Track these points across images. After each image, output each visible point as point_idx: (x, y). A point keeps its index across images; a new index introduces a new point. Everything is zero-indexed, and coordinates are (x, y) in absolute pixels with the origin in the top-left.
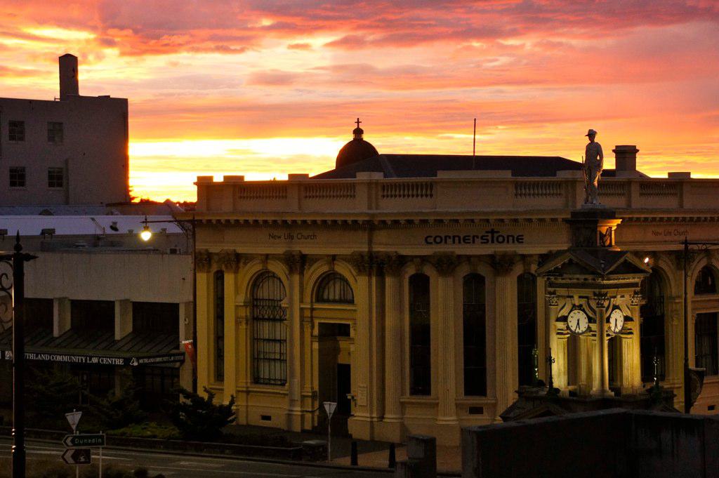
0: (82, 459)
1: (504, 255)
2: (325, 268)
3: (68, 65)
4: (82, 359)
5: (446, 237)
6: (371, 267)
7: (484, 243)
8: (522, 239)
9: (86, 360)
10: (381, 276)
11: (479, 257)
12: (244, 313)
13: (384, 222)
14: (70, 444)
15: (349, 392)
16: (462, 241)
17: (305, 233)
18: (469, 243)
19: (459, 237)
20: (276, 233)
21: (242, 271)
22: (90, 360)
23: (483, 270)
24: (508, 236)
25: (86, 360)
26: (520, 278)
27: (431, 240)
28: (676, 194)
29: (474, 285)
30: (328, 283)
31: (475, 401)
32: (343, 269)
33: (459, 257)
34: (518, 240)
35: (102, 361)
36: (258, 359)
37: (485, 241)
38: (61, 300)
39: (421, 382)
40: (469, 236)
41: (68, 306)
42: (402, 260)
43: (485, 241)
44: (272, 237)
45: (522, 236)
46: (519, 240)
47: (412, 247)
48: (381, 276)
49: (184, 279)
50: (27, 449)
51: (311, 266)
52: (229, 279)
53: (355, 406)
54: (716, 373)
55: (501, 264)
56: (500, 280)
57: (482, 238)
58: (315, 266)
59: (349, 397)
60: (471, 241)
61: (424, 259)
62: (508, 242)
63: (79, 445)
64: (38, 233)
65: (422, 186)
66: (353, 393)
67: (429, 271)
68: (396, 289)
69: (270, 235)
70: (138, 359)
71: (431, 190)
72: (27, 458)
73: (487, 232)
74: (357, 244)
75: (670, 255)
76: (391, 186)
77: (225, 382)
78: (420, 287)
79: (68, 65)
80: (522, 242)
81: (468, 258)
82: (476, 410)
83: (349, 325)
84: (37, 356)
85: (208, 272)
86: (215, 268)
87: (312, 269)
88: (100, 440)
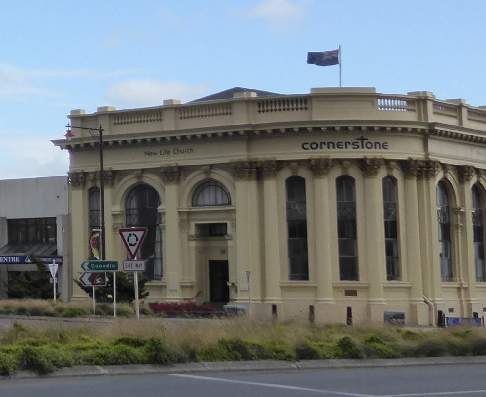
0: (98, 281)
1: (319, 160)
2: (202, 177)
5: (321, 143)
7: (356, 148)
8: (387, 146)
12: (121, 221)
14: (87, 268)
16: (336, 146)
17: (183, 147)
18: (342, 148)
19: (379, 144)
20: (152, 150)
23: (303, 173)
24: (376, 143)
26: (384, 180)
27: (306, 146)
31: (350, 284)
32: (220, 176)
33: (334, 160)
34: (383, 146)
37: (355, 144)
40: (342, 142)
42: (280, 165)
43: (356, 147)
44: (148, 154)
45: (387, 143)
46: (384, 146)
49: (58, 197)
52: (107, 192)
54: (484, 281)
56: (369, 181)
60: (344, 147)
61: (300, 162)
63: (95, 269)
67: (354, 172)
69: (146, 152)
71: (306, 104)
73: (357, 139)
75: (184, 300)
77: (461, 98)
81: (340, 162)
82: (351, 293)
83: (226, 224)
85: (83, 188)
88: (114, 266)
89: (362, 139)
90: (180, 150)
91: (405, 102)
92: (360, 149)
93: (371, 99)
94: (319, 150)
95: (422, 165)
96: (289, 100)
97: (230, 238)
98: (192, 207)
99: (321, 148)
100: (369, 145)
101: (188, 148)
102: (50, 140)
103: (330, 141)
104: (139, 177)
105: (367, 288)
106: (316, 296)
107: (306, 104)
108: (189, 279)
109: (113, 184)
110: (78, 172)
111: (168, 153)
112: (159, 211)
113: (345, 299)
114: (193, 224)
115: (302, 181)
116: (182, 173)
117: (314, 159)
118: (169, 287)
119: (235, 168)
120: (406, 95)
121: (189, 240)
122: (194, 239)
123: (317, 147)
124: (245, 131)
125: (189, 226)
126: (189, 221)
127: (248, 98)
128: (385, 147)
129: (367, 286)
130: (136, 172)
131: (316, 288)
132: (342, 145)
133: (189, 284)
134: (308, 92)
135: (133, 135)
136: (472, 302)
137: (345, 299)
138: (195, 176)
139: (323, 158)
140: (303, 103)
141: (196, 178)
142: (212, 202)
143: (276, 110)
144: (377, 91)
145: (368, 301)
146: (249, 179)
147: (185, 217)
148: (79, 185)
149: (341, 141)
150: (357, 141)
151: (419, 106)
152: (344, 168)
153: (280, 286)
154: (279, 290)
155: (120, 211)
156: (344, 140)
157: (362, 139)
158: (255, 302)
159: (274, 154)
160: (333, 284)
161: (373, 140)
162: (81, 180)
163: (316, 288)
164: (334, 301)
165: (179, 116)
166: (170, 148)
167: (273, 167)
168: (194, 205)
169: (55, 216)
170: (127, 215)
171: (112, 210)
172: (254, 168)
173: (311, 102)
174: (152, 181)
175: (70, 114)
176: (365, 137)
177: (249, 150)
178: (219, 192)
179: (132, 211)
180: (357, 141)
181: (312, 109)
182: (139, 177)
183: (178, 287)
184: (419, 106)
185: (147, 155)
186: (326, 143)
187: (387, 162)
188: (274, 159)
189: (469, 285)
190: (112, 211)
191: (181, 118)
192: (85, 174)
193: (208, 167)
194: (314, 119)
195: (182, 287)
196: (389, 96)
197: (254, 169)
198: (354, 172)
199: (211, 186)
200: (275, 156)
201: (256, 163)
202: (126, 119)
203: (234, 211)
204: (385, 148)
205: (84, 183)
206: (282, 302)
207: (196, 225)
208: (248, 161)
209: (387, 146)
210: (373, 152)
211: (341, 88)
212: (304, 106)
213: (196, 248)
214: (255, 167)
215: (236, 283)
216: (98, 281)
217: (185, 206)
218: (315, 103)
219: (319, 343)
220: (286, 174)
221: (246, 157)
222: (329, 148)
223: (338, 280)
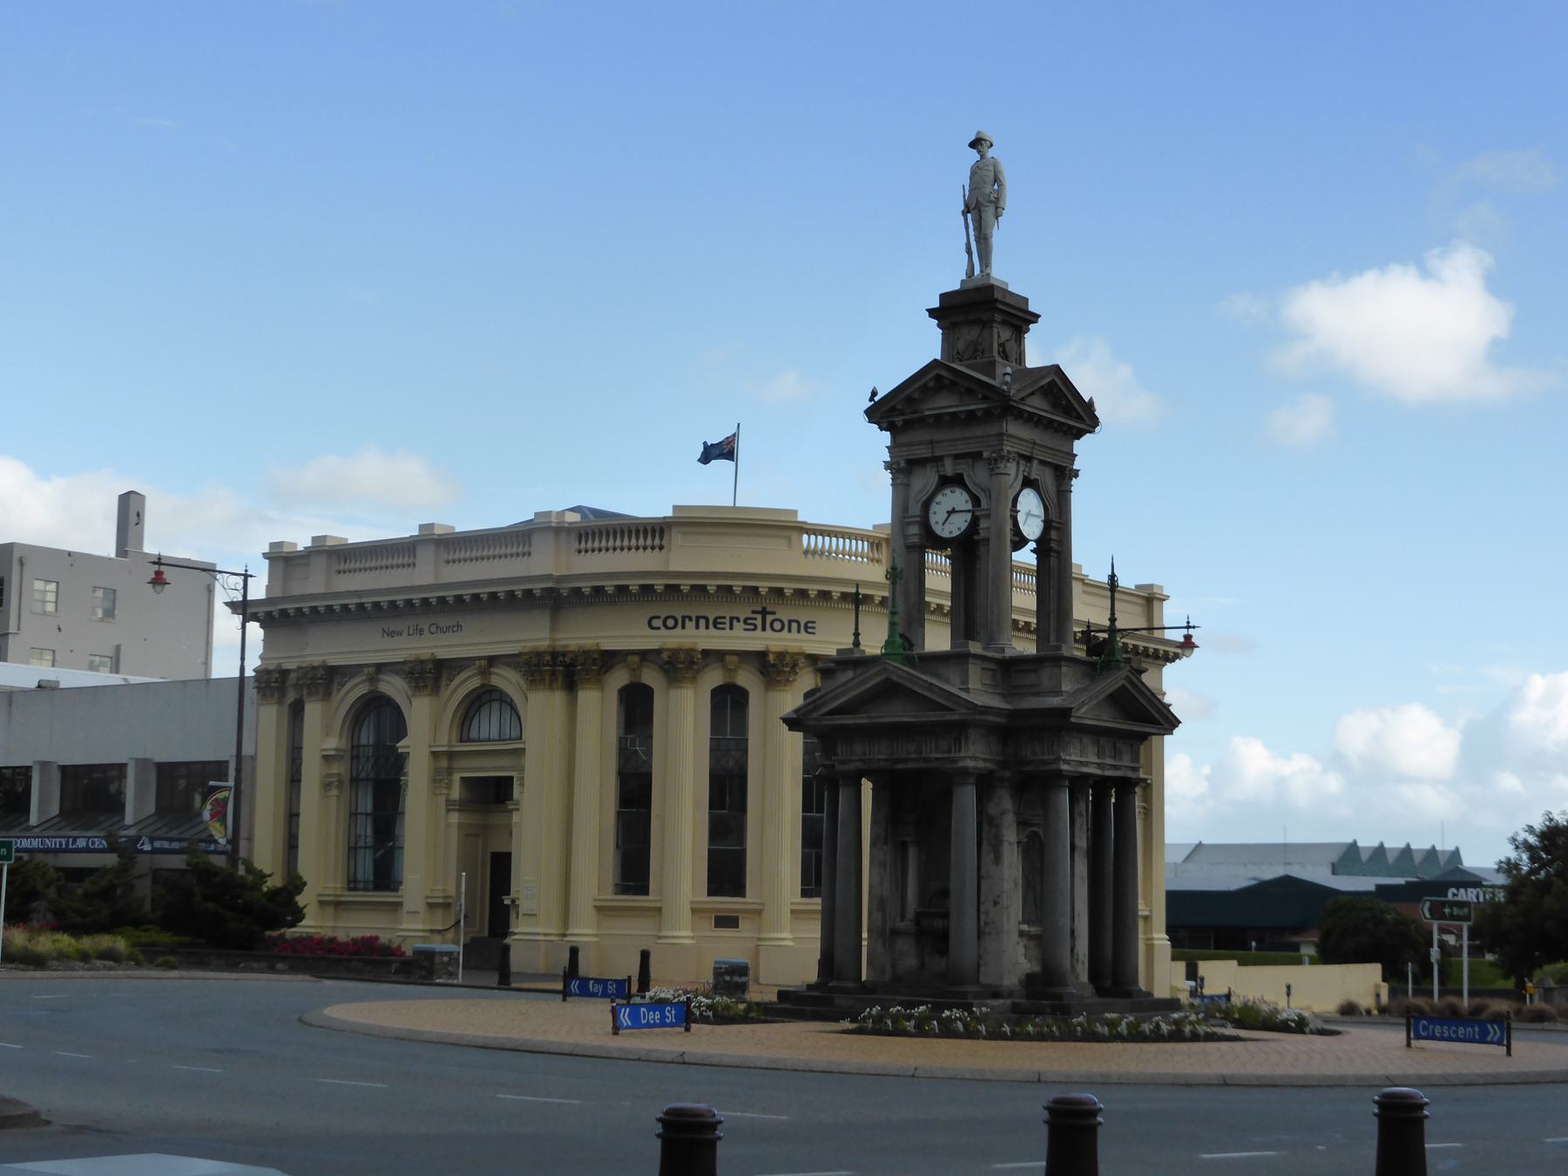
1: (675, 652)
2: (475, 683)
3: (130, 510)
4: (61, 844)
5: (684, 618)
6: (553, 673)
8: (814, 628)
9: (67, 843)
10: (571, 687)
11: (744, 656)
13: (577, 591)
15: (508, 893)
17: (444, 621)
18: (724, 629)
19: (707, 619)
22: (74, 842)
23: (651, 677)
24: (790, 622)
25: (67, 843)
27: (656, 623)
30: (479, 710)
31: (725, 903)
32: (508, 680)
33: (705, 653)
35: (93, 843)
36: (356, 848)
37: (749, 621)
38: (45, 765)
40: (724, 618)
41: (56, 777)
42: (608, 660)
43: (752, 627)
45: (814, 622)
46: (808, 627)
48: (571, 687)
52: (313, 711)
56: (673, 692)
57: (745, 622)
59: (507, 902)
61: (645, 656)
62: (790, 631)
64: (34, 685)
66: (513, 895)
67: (746, 679)
70: (152, 840)
71: (661, 538)
72: (1426, 1146)
73: (754, 612)
74: (532, 634)
79: (130, 510)
80: (814, 633)
82: (727, 921)
85: (280, 702)
86: (291, 696)
89: (764, 612)
90: (442, 626)
91: (866, 543)
92: (759, 632)
93: (783, 533)
94: (678, 630)
95: (596, 656)
96: (632, 528)
97: (516, 807)
98: (460, 744)
99: (683, 627)
100: (777, 625)
101: (452, 622)
103: (699, 614)
104: (373, 680)
105: (759, 912)
106: (660, 930)
107: (661, 538)
108: (444, 890)
109: (327, 695)
110: (271, 668)
111: (421, 632)
112: (400, 751)
113: (714, 934)
114: (457, 777)
115: (648, 692)
116: (445, 675)
117: (667, 650)
118: (406, 908)
119: (528, 663)
120: (871, 529)
121: (448, 811)
122: (457, 807)
123: (675, 626)
124: (543, 589)
125: (451, 781)
126: (450, 771)
127: (557, 523)
128: (809, 630)
129: (759, 907)
130: (366, 670)
131: (659, 910)
132: (724, 623)
133: (441, 901)
134: (669, 513)
135: (357, 594)
136: (1155, 942)
137: (714, 934)
138: (466, 680)
139: (790, 651)
140: (626, 537)
141: (466, 683)
142: (494, 734)
143: (653, 548)
144: (801, 518)
145: (760, 939)
146: (551, 688)
147: (444, 763)
148: (272, 695)
149: (657, 615)
150: (754, 616)
152: (730, 671)
153: (595, 907)
154: (593, 912)
155: (336, 749)
156: (727, 612)
157: (764, 612)
158: (547, 938)
159: (596, 638)
160: (692, 902)
161: (784, 614)
162: (273, 685)
163: (659, 910)
164: (693, 938)
165: (446, 557)
166: (424, 623)
167: (595, 664)
168: (465, 738)
169: (227, 759)
170: (352, 758)
171: (325, 747)
172: (559, 666)
173: (671, 536)
174: (394, 687)
175: (267, 550)
176: (769, 609)
177: (554, 627)
178: (507, 711)
179: (361, 749)
180: (754, 616)
181: (670, 550)
182: (373, 680)
183: (420, 906)
185: (385, 635)
186: (694, 619)
188: (595, 648)
189: (1151, 911)
190: (322, 750)
191: (448, 562)
192: (284, 673)
193: (483, 663)
194: (673, 568)
195: (431, 906)
196: (847, 530)
197: (561, 668)
198: (746, 679)
199: (494, 700)
200: (802, 644)
201: (564, 654)
202: (363, 561)
203: (523, 750)
204: (809, 633)
205: (282, 691)
206: (597, 939)
207: (463, 779)
208: (550, 649)
209: (814, 628)
210: (680, 637)
211: (735, 509)
212: (657, 542)
213: (460, 826)
214: (561, 662)
215: (518, 899)
217: (446, 739)
218: (676, 538)
219: (1204, 1030)
220: (713, 678)
221: (547, 643)
222: (697, 627)
223: (704, 897)
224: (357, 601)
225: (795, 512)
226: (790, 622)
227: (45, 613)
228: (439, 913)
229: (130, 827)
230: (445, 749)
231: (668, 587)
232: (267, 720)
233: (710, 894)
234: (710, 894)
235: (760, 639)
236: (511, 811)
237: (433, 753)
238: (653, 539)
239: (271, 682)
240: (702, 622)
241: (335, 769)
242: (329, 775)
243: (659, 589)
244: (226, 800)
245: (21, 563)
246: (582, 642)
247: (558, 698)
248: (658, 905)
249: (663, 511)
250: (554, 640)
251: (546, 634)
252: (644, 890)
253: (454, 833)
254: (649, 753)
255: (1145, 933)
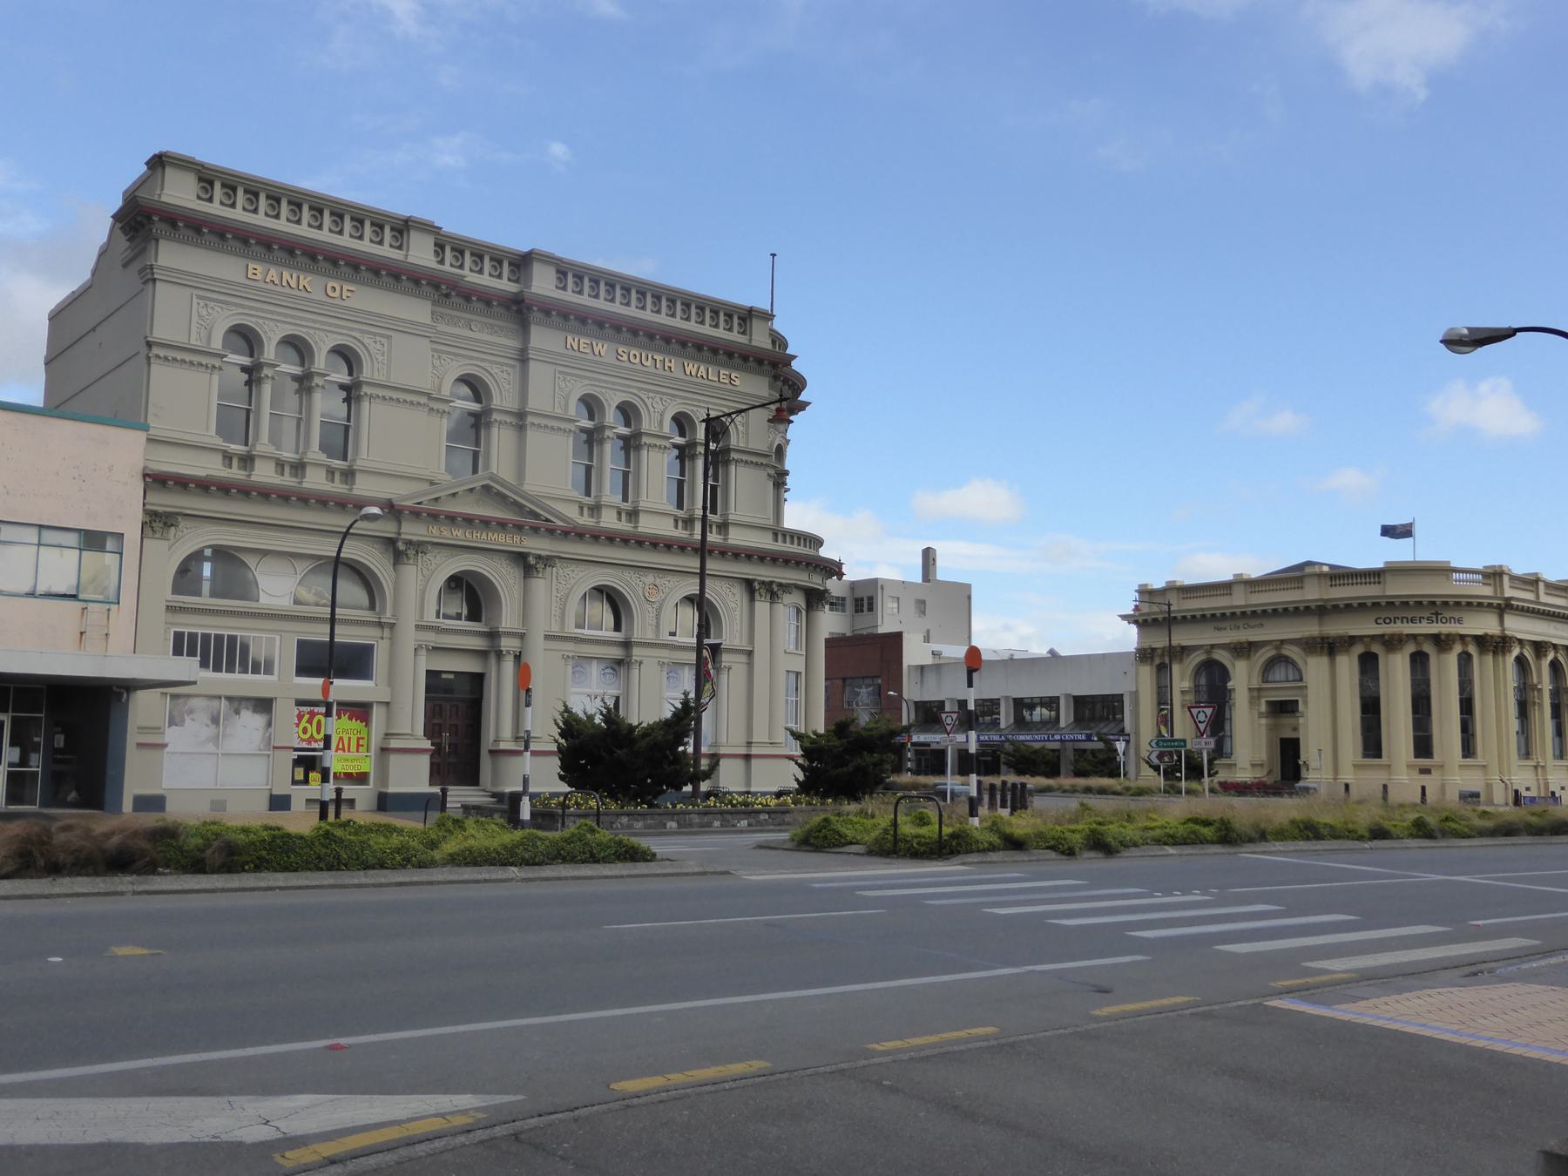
0: (1166, 759)
1: (1392, 636)
2: (1273, 653)
3: (928, 556)
14: (1154, 746)
17: (1253, 622)
21: (1254, 658)
22: (1053, 736)
23: (1376, 648)
24: (1450, 618)
26: (1460, 655)
27: (1379, 621)
28: (1490, 585)
29: (1419, 661)
32: (1292, 652)
33: (1407, 635)
38: (1007, 698)
39: (1372, 745)
42: (1352, 640)
46: (1459, 621)
47: (1366, 627)
50: (696, 568)
51: (1257, 652)
53: (1308, 770)
55: (1443, 643)
56: (1444, 656)
58: (1261, 652)
61: (1373, 638)
63: (1164, 747)
65: (1352, 575)
67: (1428, 648)
68: (1347, 665)
74: (1310, 628)
76: (1335, 577)
78: (1369, 664)
81: (1414, 637)
82: (1425, 771)
84: (1000, 737)
85: (1151, 664)
87: (1258, 655)
89: (1437, 614)
92: (1435, 624)
93: (1446, 573)
94: (1448, 625)
99: (1395, 623)
100: (1444, 620)
102: (810, 403)
104: (1208, 652)
114: (1263, 701)
115: (1375, 657)
116: (1253, 649)
119: (1307, 643)
126: (1259, 698)
131: (1389, 766)
135: (1202, 609)
138: (1265, 653)
142: (1283, 678)
147: (1255, 694)
151: (1495, 580)
152: (1418, 644)
154: (1352, 768)
156: (1418, 614)
161: (1448, 615)
163: (1389, 766)
165: (1250, 590)
166: (1241, 623)
168: (1265, 681)
174: (1222, 656)
177: (1320, 625)
181: (1385, 583)
182: (1208, 652)
183: (1248, 766)
184: (1495, 580)
187: (1462, 637)
192: (1153, 650)
194: (1388, 593)
195: (1253, 765)
198: (1428, 648)
201: (1328, 638)
203: (1306, 687)
205: (1152, 659)
211: (1415, 562)
213: (1267, 725)
216: (1166, 759)
217: (1256, 683)
218: (1389, 578)
220: (1359, 649)
224: (1201, 613)
225: (1449, 562)
226: (1450, 618)
227: (894, 614)
228: (1258, 769)
229: (1063, 728)
230: (1257, 687)
231: (1360, 604)
232: (1147, 673)
233: (1416, 757)
234: (1416, 757)
235: (1434, 627)
236: (1298, 717)
237: (1250, 689)
238: (1374, 578)
239: (1144, 655)
240: (1405, 620)
241: (1187, 698)
242: (1184, 701)
243: (1369, 605)
244: (1166, 715)
245: (882, 588)
246: (1339, 632)
247: (1324, 661)
248: (1388, 763)
249: (1380, 565)
250: (1321, 631)
251: (1317, 628)
252: (1379, 756)
253: (1264, 730)
254: (1378, 686)
255: (1542, 775)
